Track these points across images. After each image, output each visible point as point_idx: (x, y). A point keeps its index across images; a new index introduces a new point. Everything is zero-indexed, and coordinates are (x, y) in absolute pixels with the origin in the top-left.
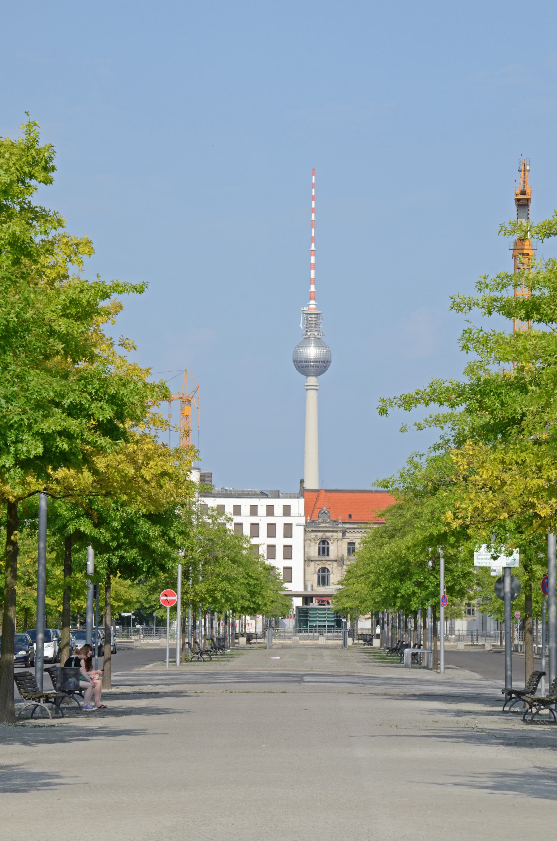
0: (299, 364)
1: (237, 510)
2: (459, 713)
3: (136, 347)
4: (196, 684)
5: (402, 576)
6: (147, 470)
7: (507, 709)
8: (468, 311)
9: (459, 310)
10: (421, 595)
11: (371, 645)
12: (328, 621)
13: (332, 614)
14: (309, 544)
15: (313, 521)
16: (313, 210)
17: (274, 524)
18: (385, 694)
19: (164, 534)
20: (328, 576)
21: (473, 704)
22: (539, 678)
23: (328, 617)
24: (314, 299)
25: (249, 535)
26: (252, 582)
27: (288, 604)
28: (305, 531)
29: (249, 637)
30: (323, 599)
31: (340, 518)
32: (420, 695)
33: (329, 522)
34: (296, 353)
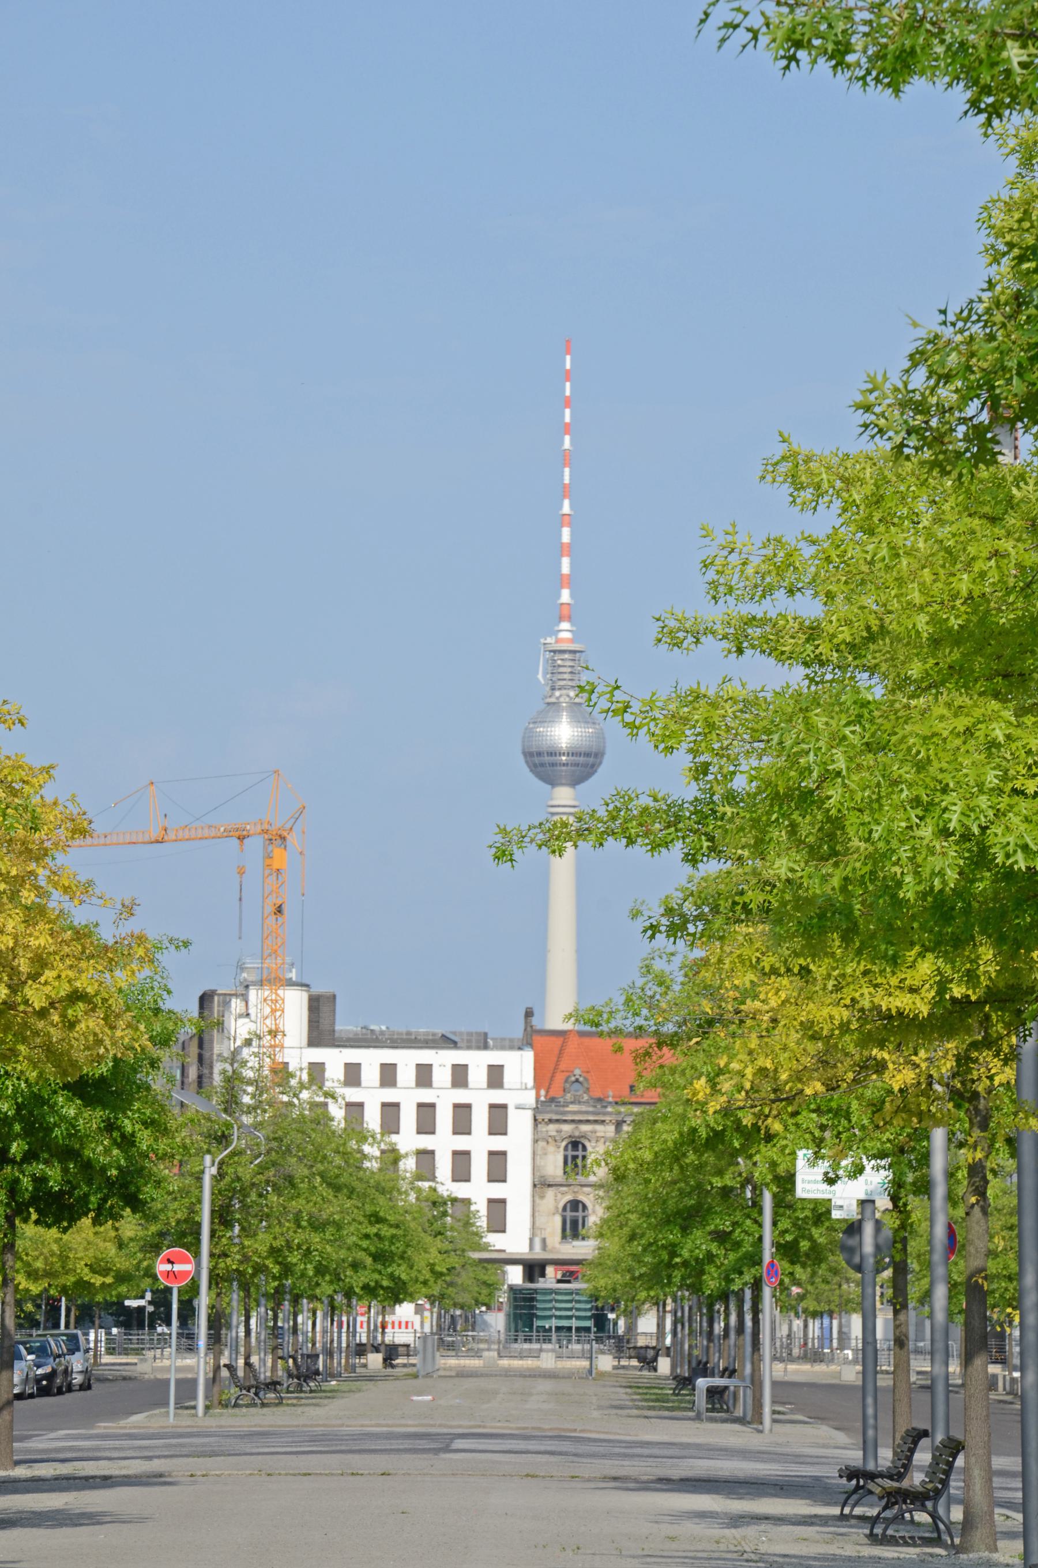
0: (536, 760)
1: (353, 1075)
2: (737, 1520)
3: (25, 722)
4: (205, 1456)
5: (685, 1219)
6: (37, 989)
7: (847, 1510)
8: (693, 646)
9: (674, 645)
10: (726, 1262)
11: (655, 1369)
12: (578, 1318)
13: (586, 1302)
14: (544, 1149)
15: (552, 1100)
16: (567, 429)
17: (468, 1107)
18: (605, 1478)
19: (110, 1127)
20: (584, 1218)
21: (788, 1501)
22: (915, 1443)
23: (578, 1310)
24: (569, 619)
25: (378, 1130)
26: (386, 1231)
27: (491, 1279)
28: (535, 1120)
29: (391, 1353)
30: (570, 1269)
31: (611, 1093)
32: (682, 1480)
33: (586, 1102)
34: (528, 735)
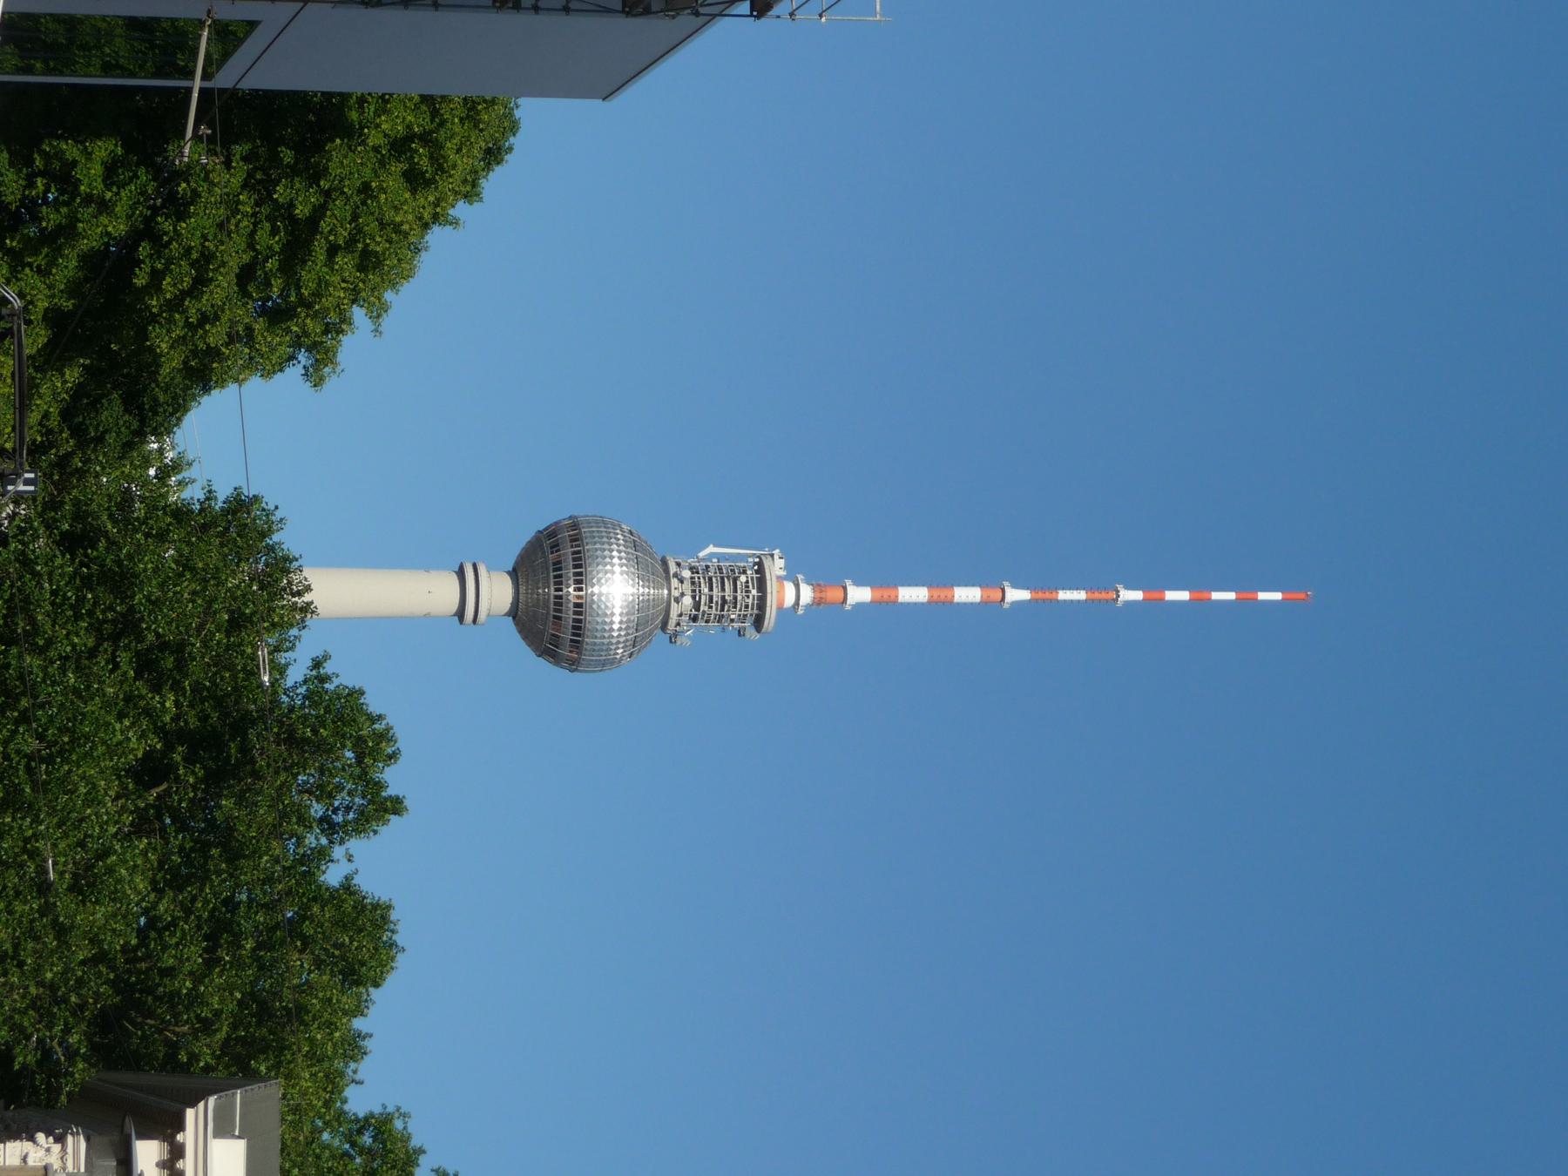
34: (606, 526)
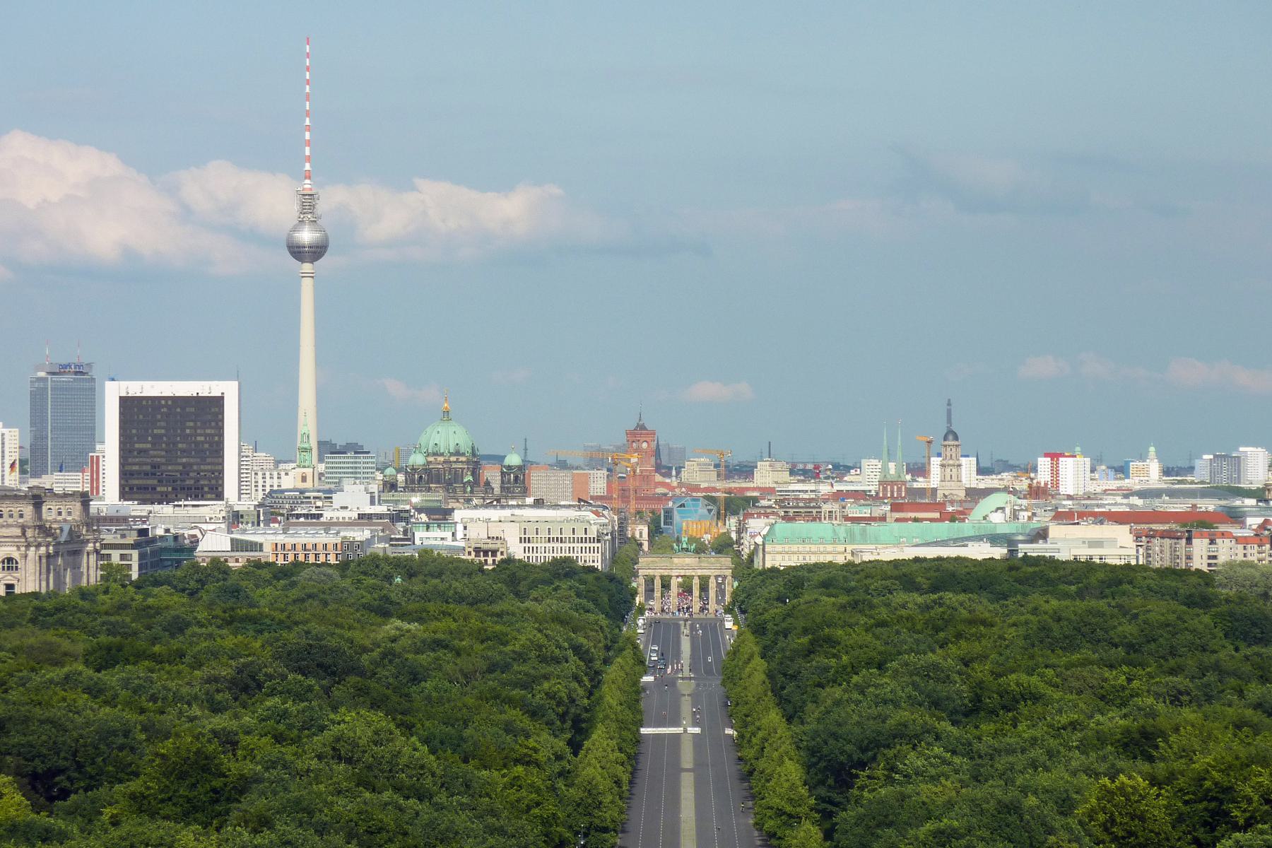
24: (310, 178)
